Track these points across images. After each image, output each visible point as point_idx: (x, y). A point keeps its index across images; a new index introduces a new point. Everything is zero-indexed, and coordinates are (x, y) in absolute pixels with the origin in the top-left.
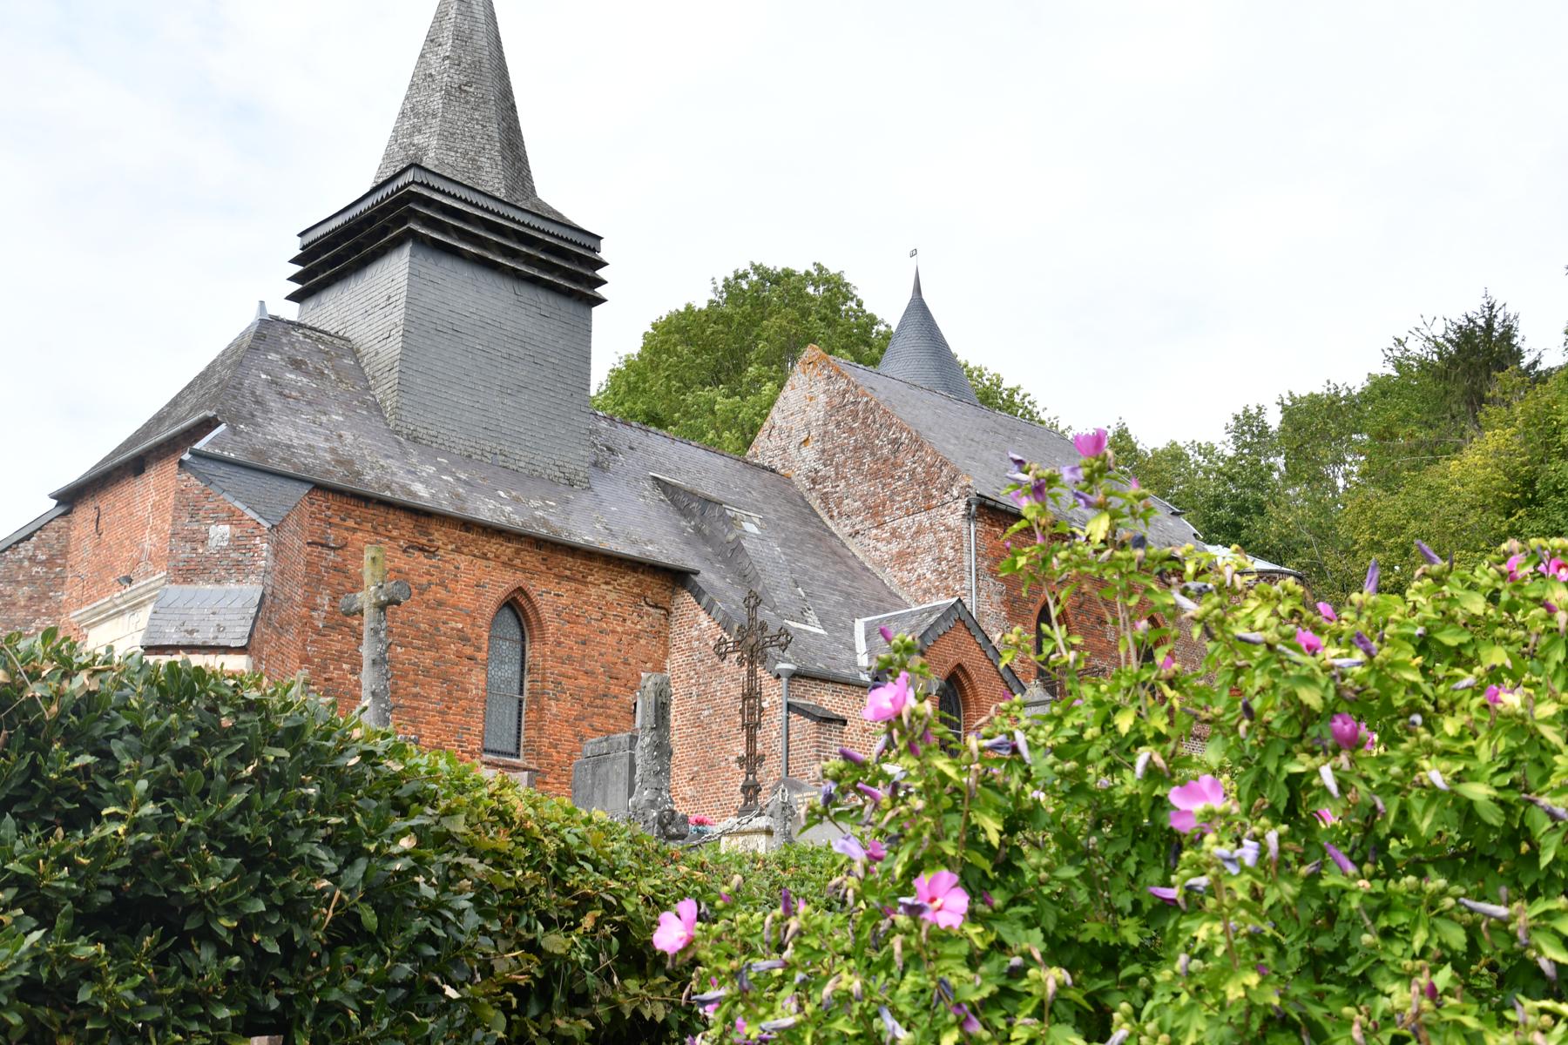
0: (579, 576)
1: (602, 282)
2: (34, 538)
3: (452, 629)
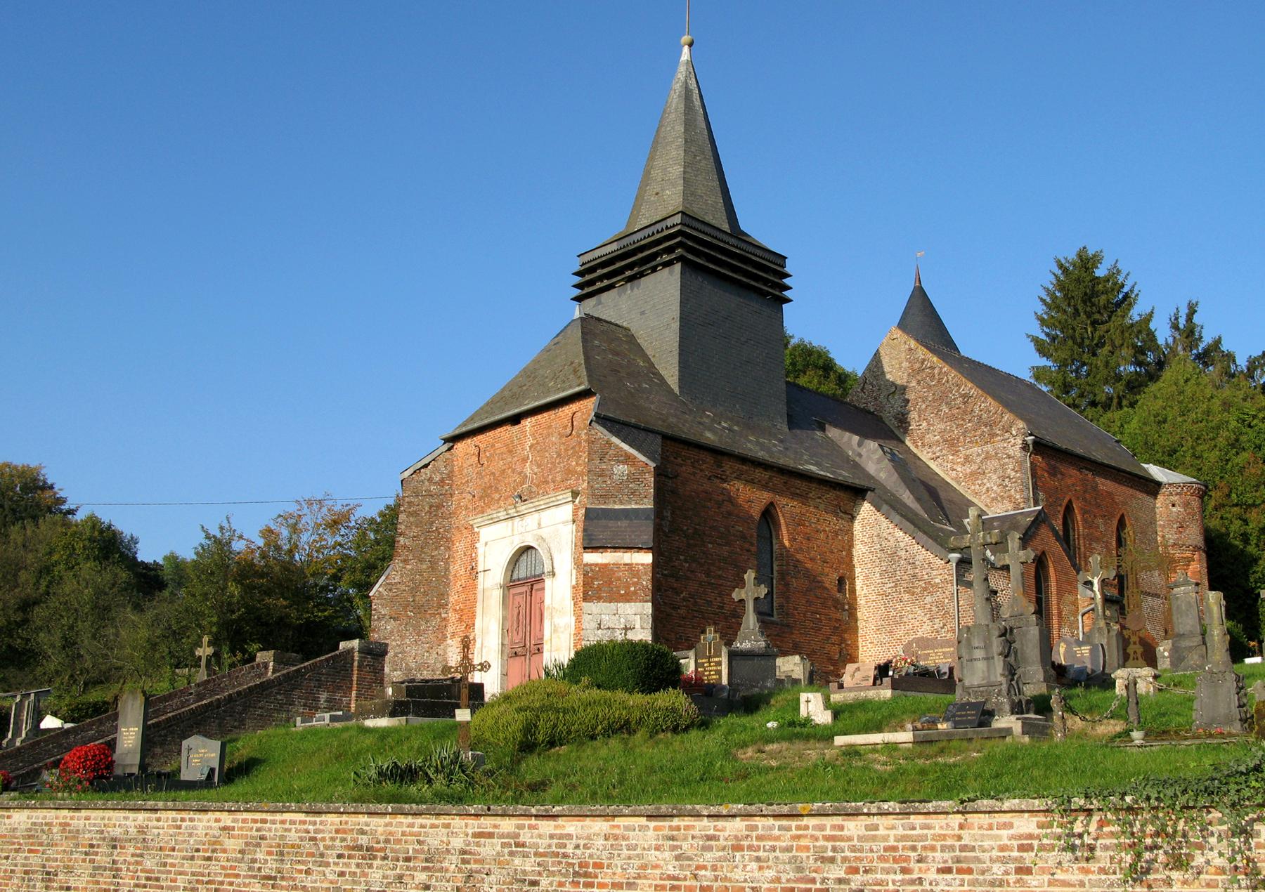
0: (804, 494)
3: (738, 531)
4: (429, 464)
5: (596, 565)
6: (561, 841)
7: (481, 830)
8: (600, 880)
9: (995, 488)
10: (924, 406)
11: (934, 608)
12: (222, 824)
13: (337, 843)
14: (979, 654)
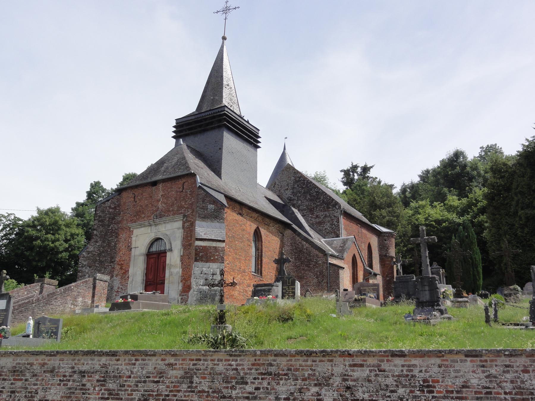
1: (259, 142)
2: (110, 201)
4: (109, 200)
5: (201, 246)
6: (409, 368)
7: (354, 363)
8: (437, 389)
9: (329, 228)
10: (300, 195)
11: (318, 273)
12: (167, 362)
13: (253, 371)
14: (427, 288)
